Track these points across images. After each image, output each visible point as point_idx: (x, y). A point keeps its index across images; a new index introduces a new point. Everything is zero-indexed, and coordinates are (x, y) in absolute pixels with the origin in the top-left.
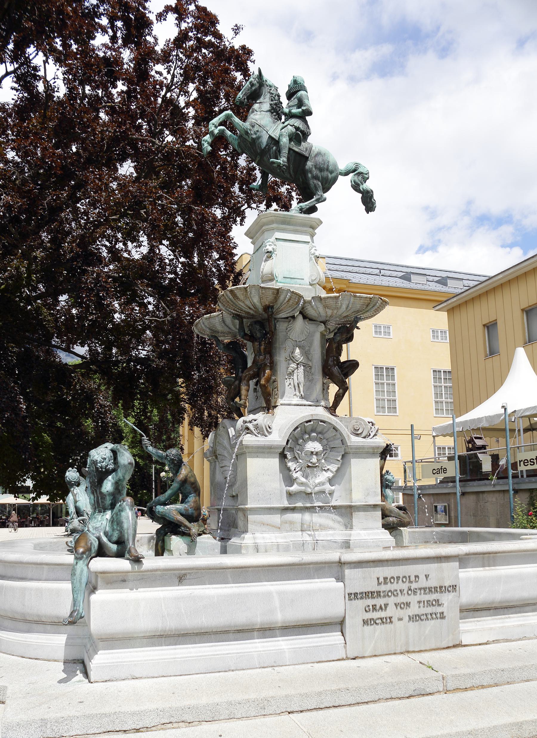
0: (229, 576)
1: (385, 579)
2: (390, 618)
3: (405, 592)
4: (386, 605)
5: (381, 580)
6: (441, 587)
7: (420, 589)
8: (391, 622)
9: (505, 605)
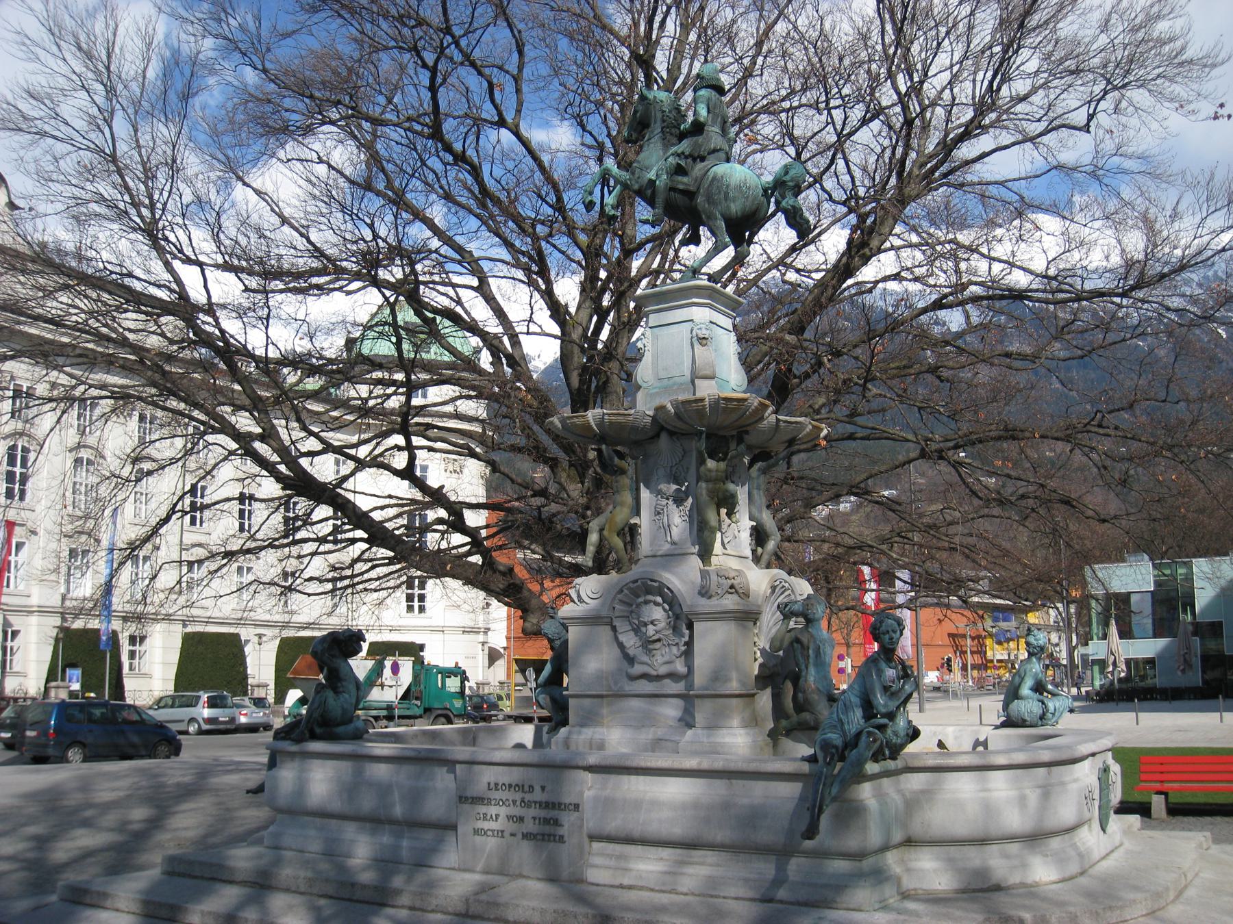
5: (492, 786)
7: (535, 802)
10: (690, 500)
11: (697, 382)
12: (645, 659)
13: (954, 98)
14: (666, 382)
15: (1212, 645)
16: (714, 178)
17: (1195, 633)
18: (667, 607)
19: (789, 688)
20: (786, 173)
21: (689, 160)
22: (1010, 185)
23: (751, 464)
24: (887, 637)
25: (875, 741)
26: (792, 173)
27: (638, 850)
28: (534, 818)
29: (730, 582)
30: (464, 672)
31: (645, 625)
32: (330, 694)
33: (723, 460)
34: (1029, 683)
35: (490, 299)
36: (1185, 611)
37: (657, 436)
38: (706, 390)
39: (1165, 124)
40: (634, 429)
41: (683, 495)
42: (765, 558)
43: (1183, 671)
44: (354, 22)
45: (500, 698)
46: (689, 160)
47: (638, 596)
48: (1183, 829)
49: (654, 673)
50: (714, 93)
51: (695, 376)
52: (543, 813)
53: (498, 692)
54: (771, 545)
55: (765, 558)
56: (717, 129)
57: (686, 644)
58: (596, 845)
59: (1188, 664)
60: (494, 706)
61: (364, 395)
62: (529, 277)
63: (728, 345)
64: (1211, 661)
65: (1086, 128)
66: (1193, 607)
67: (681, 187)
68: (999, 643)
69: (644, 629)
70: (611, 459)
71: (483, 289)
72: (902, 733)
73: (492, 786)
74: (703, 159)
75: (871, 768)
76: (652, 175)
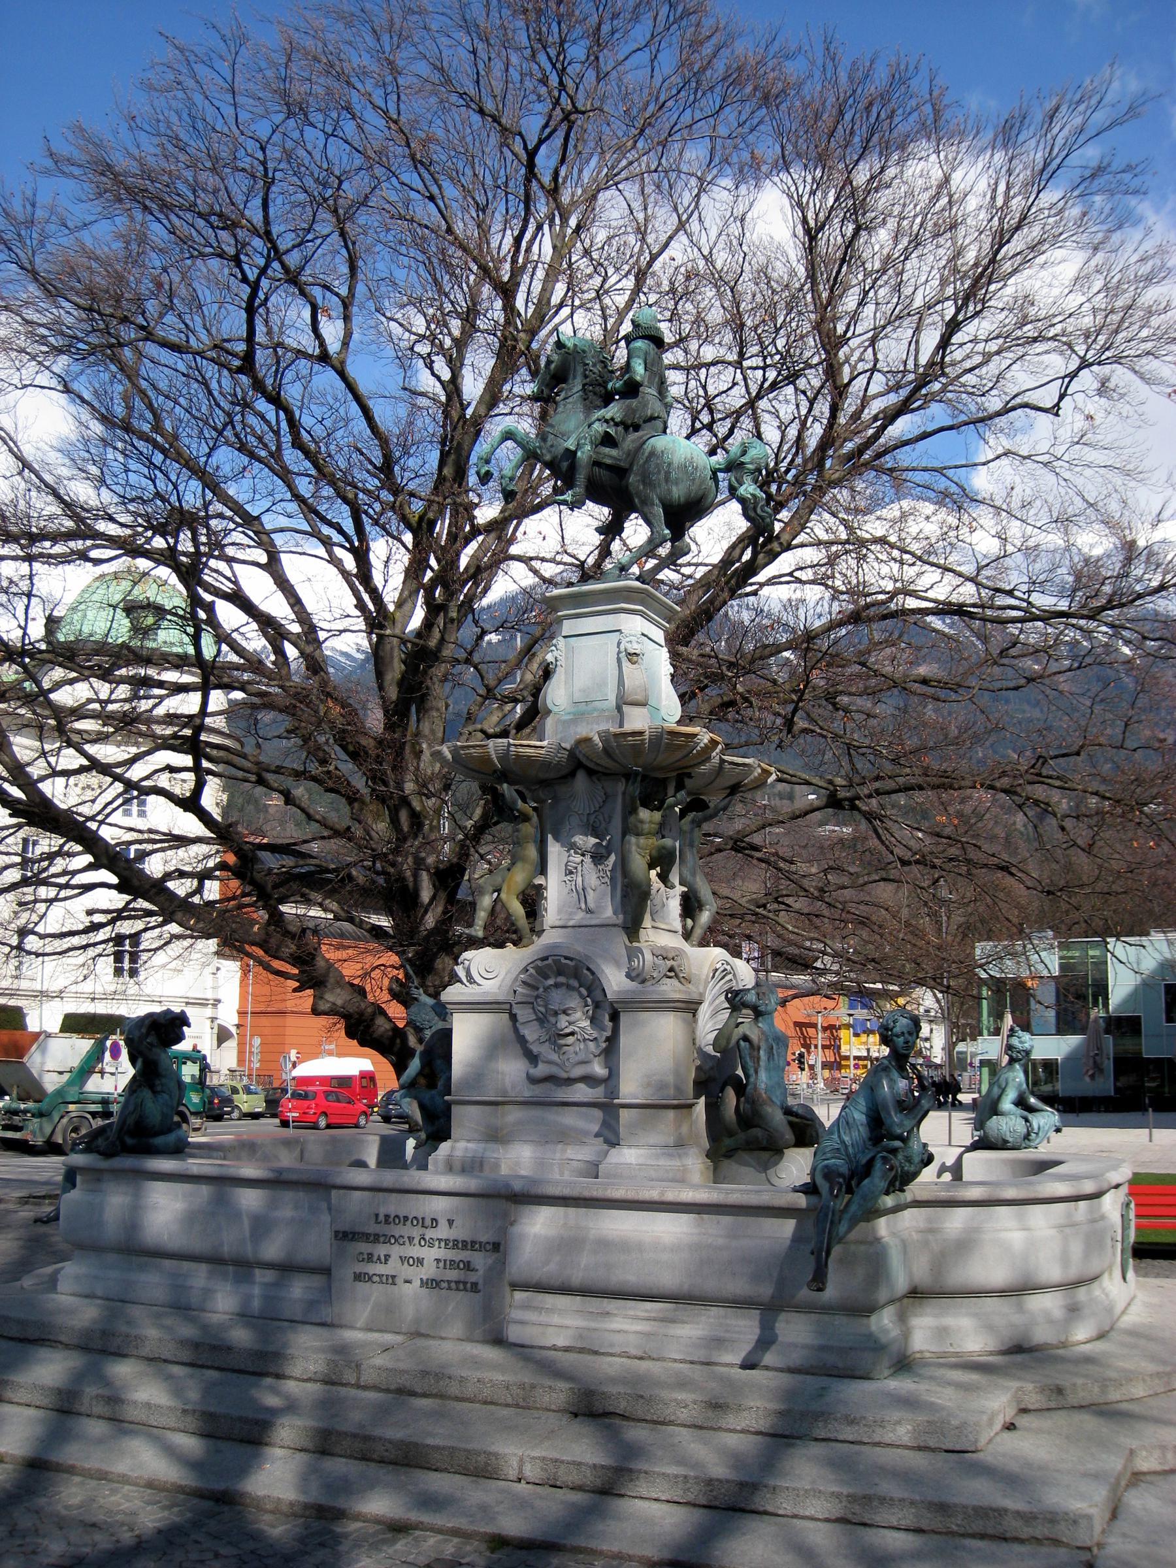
0: (471, 1145)
1: (387, 1216)
2: (393, 1277)
3: (416, 1241)
4: (387, 1257)
5: (381, 1218)
6: (473, 1243)
7: (440, 1240)
8: (394, 1284)
9: (643, 1291)
10: (613, 858)
11: (625, 708)
12: (554, 1057)
13: (876, 361)
14: (582, 707)
15: (1128, 1044)
16: (652, 454)
17: (1107, 1032)
18: (584, 991)
19: (730, 1096)
20: (744, 453)
21: (620, 429)
22: (950, 473)
23: (683, 813)
24: (901, 1039)
25: (891, 1169)
26: (752, 453)
27: (550, 1300)
28: (438, 1260)
29: (669, 963)
30: (204, 1058)
31: (556, 1014)
32: (147, 1094)
33: (658, 809)
34: (1011, 1095)
35: (283, 584)
36: (1096, 1004)
37: (572, 774)
38: (637, 720)
39: (1141, 409)
40: (545, 764)
41: (603, 851)
42: (698, 932)
43: (1092, 1077)
44: (161, 216)
45: (235, 1090)
46: (620, 429)
47: (546, 977)
48: (1157, 1276)
49: (564, 1075)
50: (652, 346)
51: (623, 702)
52: (450, 1254)
53: (230, 1083)
54: (705, 917)
55: (698, 932)
56: (653, 391)
57: (608, 1039)
58: (519, 1296)
59: (1098, 1068)
60: (228, 1101)
61: (104, 696)
62: (330, 552)
63: (660, 662)
64: (1127, 1064)
65: (1055, 410)
66: (1106, 999)
67: (608, 461)
68: (856, 1035)
69: (553, 1020)
70: (515, 802)
71: (273, 567)
72: (917, 1159)
73: (381, 1218)
74: (637, 428)
75: (889, 1201)
76: (571, 444)
